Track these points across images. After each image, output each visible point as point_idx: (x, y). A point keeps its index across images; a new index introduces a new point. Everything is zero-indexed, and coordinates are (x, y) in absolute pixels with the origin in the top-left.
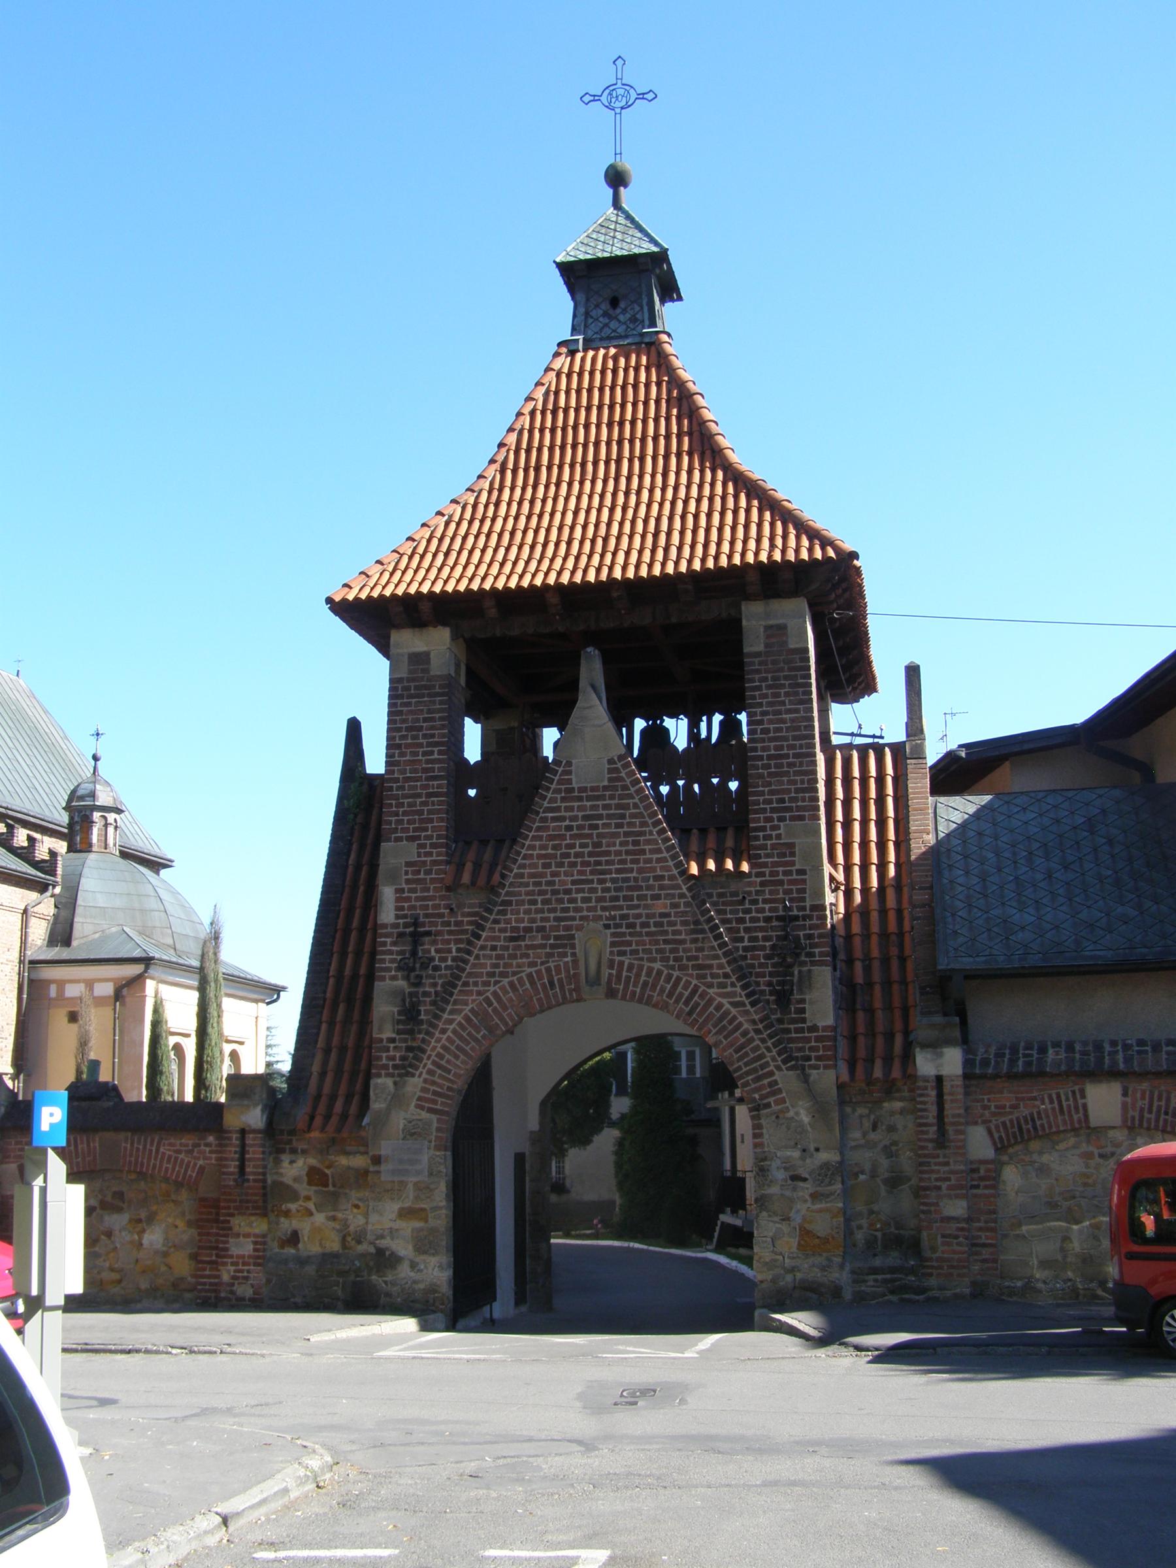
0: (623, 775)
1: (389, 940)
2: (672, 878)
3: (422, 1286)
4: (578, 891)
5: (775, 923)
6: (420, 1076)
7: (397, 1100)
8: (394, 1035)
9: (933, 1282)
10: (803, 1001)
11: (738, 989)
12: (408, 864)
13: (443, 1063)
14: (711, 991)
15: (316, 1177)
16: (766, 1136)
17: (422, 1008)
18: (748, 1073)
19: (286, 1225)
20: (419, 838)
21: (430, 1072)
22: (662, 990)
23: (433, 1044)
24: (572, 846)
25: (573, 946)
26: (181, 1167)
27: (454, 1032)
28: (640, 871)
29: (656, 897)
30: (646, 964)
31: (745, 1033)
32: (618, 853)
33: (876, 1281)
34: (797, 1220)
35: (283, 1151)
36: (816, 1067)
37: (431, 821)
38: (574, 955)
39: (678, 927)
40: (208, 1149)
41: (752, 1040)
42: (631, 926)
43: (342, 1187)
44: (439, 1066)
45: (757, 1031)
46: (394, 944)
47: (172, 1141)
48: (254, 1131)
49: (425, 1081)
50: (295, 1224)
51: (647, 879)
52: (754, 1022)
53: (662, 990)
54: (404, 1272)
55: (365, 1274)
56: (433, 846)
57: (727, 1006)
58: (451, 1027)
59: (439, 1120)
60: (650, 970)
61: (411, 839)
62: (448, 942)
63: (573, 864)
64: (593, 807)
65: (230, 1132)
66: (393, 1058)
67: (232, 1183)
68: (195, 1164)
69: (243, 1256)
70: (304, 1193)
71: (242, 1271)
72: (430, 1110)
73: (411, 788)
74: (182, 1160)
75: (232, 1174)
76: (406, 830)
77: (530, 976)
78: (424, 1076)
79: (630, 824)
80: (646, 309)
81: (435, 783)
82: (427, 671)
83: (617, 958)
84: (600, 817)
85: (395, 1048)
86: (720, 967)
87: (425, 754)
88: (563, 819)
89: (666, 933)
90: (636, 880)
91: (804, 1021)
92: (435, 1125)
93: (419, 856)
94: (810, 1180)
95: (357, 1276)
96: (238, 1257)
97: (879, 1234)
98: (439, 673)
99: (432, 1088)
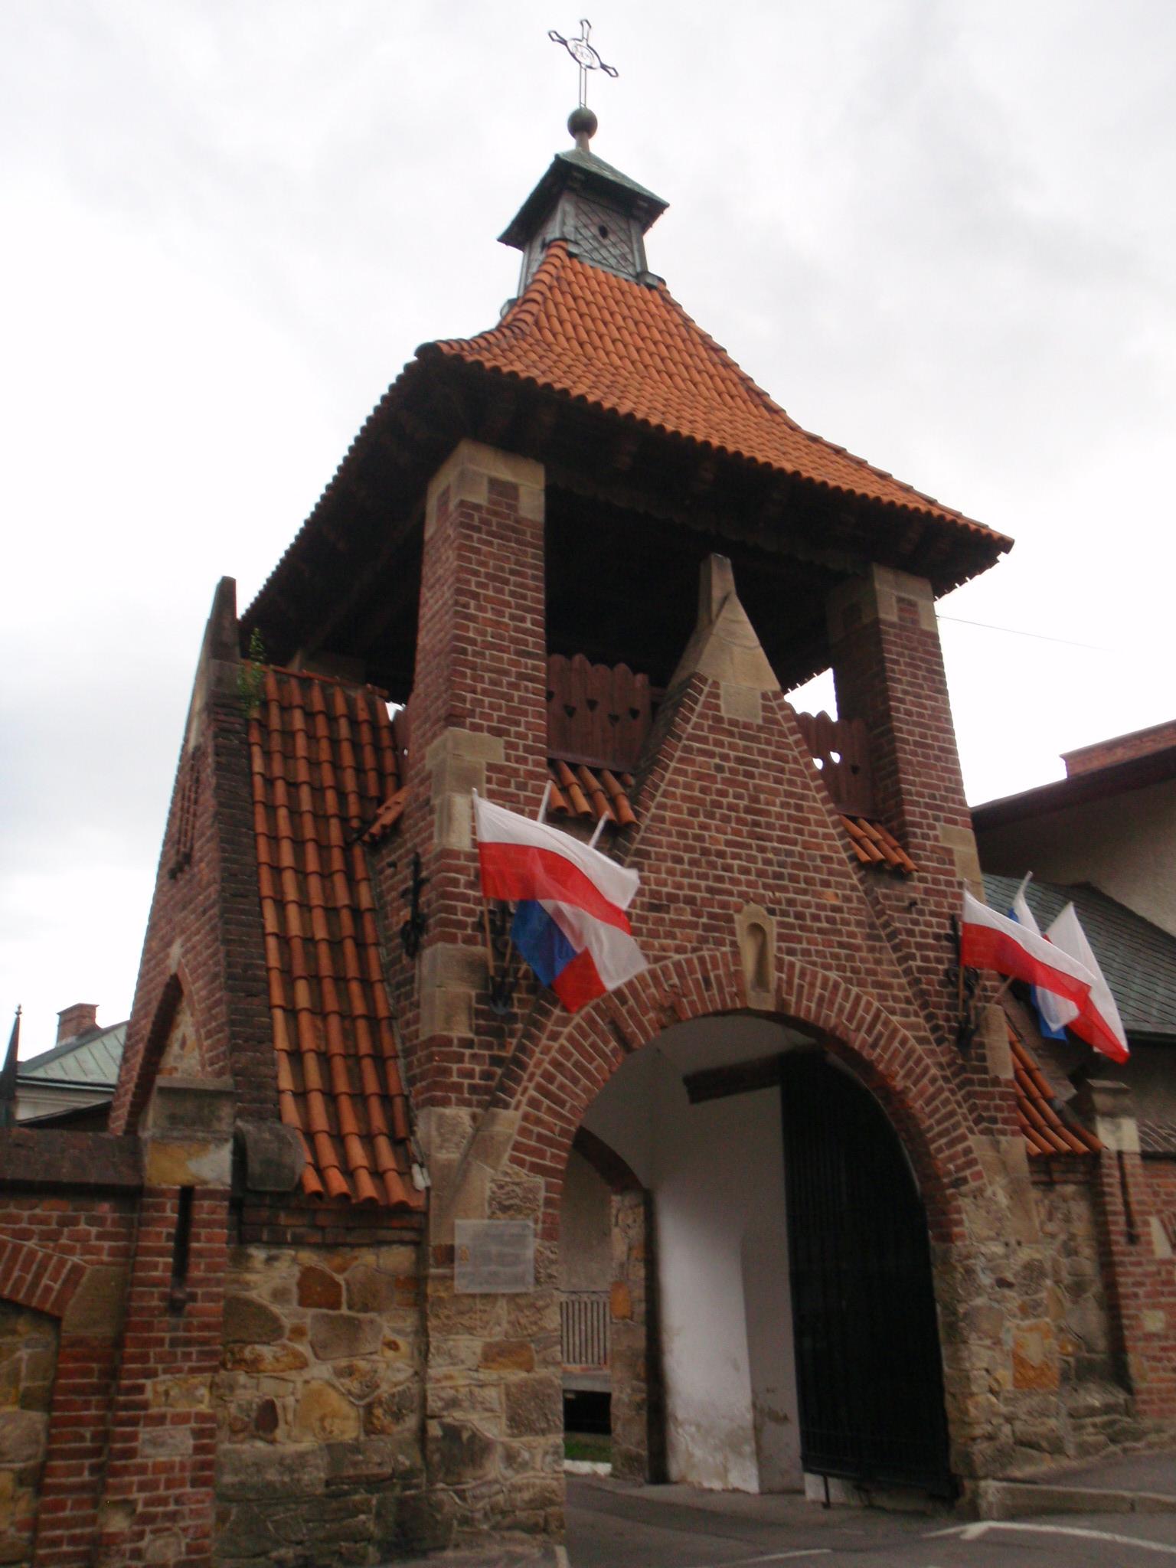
0: (779, 717)
1: (463, 878)
2: (841, 862)
3: (527, 1495)
4: (735, 856)
5: (945, 943)
6: (517, 1108)
7: (480, 1145)
8: (471, 1035)
9: (1148, 1422)
10: (982, 1045)
11: (921, 1021)
12: (491, 767)
13: (553, 1088)
14: (894, 1018)
15: (315, 1290)
16: (967, 1224)
17: (515, 995)
18: (940, 1135)
19: (248, 1391)
20: (507, 733)
21: (533, 1103)
22: (841, 1010)
23: (538, 1055)
24: (723, 793)
25: (732, 933)
26: (26, 1268)
27: (571, 1038)
28: (806, 846)
29: (826, 884)
30: (821, 972)
31: (933, 1081)
32: (779, 816)
33: (1094, 1425)
34: (1009, 1344)
36: (1003, 1133)
37: (525, 713)
38: (734, 944)
39: (853, 928)
40: (94, 1230)
41: (940, 1090)
42: (799, 916)
43: (366, 1308)
44: (547, 1094)
45: (946, 1079)
46: (470, 885)
47: (13, 1210)
48: (211, 1194)
49: (526, 1117)
50: (268, 1388)
51: (812, 858)
52: (941, 1066)
53: (841, 1010)
54: (495, 1467)
55: (423, 1479)
56: (528, 749)
57: (912, 1042)
58: (566, 1030)
59: (549, 1187)
60: (826, 980)
61: (497, 732)
63: (726, 819)
64: (747, 749)
65: (162, 1193)
66: (470, 1074)
67: (155, 1303)
68: (62, 1263)
69: (168, 1467)
70: (287, 1323)
71: (163, 1501)
72: (536, 1168)
73: (493, 658)
74: (32, 1253)
75: (157, 1282)
76: (488, 717)
77: (677, 965)
78: (524, 1108)
79: (791, 783)
80: (636, 254)
81: (530, 662)
83: (787, 958)
84: (756, 764)
85: (474, 1056)
86: (901, 988)
87: (513, 617)
88: (712, 755)
89: (839, 933)
90: (801, 855)
91: (985, 1070)
92: (542, 1194)
93: (508, 759)
94: (1016, 1288)
95: (406, 1487)
96: (159, 1468)
97: (1071, 1359)
98: (530, 516)
99: (537, 1129)
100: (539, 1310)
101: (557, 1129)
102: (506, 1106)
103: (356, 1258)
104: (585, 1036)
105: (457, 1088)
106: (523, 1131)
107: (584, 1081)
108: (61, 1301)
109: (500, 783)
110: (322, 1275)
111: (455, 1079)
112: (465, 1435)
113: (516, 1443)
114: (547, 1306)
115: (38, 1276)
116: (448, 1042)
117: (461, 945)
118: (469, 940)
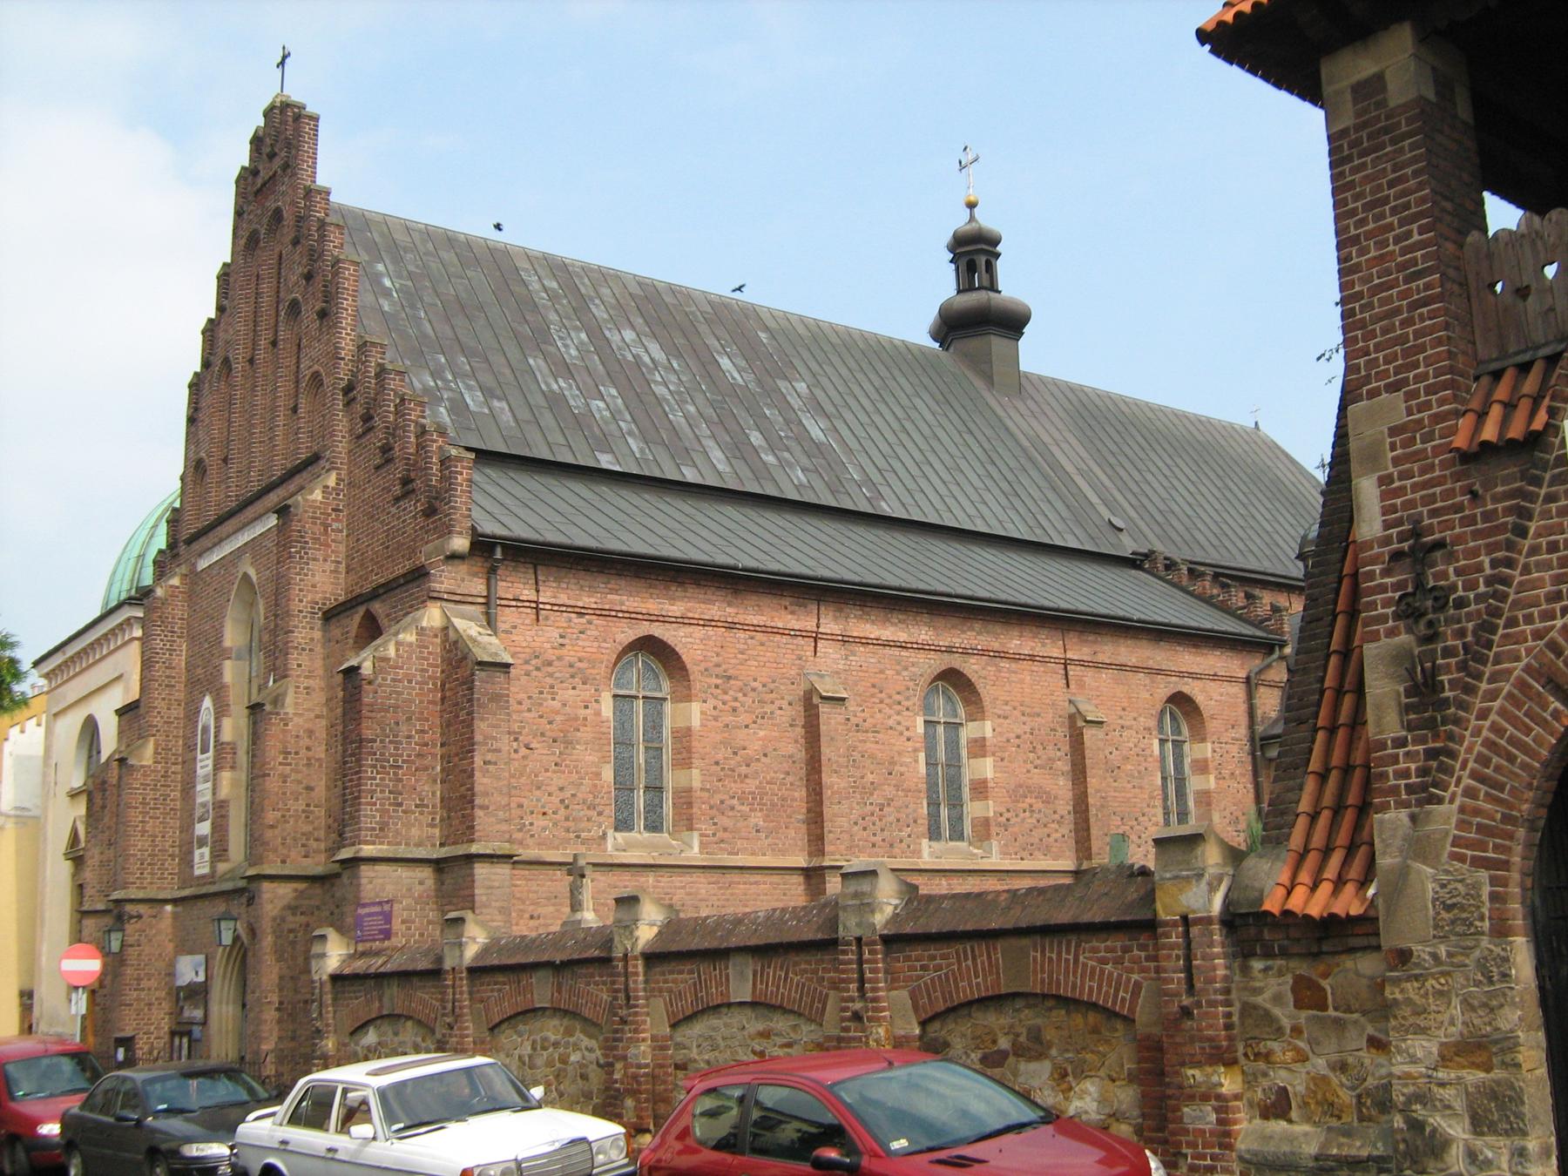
1: (1377, 568)
6: (1452, 801)
12: (1393, 431)
21: (1470, 793)
27: (1502, 712)
35: (1253, 954)
40: (1143, 954)
46: (1386, 573)
58: (1496, 704)
61: (1393, 388)
62: (1475, 553)
66: (1405, 774)
68: (1129, 980)
70: (1286, 1023)
73: (1382, 302)
82: (1381, 104)
92: (1486, 890)
100: (1492, 1010)
101: (1499, 816)
102: (1440, 801)
103: (1338, 965)
104: (1519, 706)
105: (1394, 790)
106: (1461, 824)
107: (1521, 757)
108: (1132, 1009)
109: (1404, 445)
110: (1309, 980)
111: (1393, 782)
112: (1428, 1130)
113: (1478, 1143)
114: (1502, 1006)
115: (1117, 991)
116: (1383, 746)
117: (1384, 641)
118: (1391, 633)
